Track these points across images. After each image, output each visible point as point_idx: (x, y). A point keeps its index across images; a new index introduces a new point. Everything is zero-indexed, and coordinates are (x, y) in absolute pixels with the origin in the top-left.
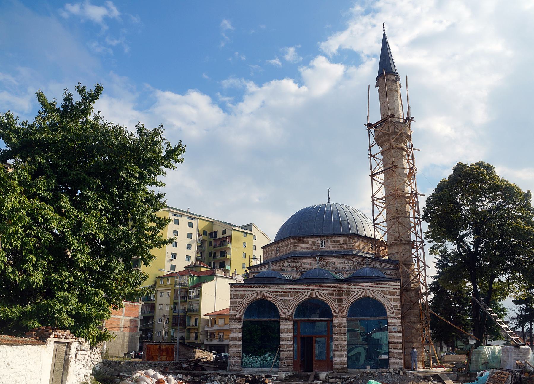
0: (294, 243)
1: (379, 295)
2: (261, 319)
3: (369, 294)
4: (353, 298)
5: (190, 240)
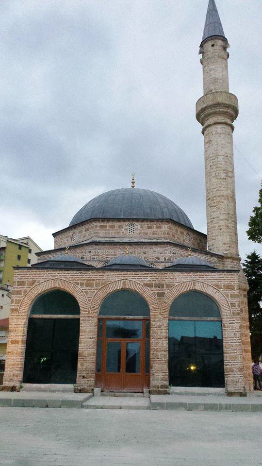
0: (96, 227)
1: (212, 289)
2: (70, 316)
3: (198, 287)
4: (175, 293)
5: (5, 296)
